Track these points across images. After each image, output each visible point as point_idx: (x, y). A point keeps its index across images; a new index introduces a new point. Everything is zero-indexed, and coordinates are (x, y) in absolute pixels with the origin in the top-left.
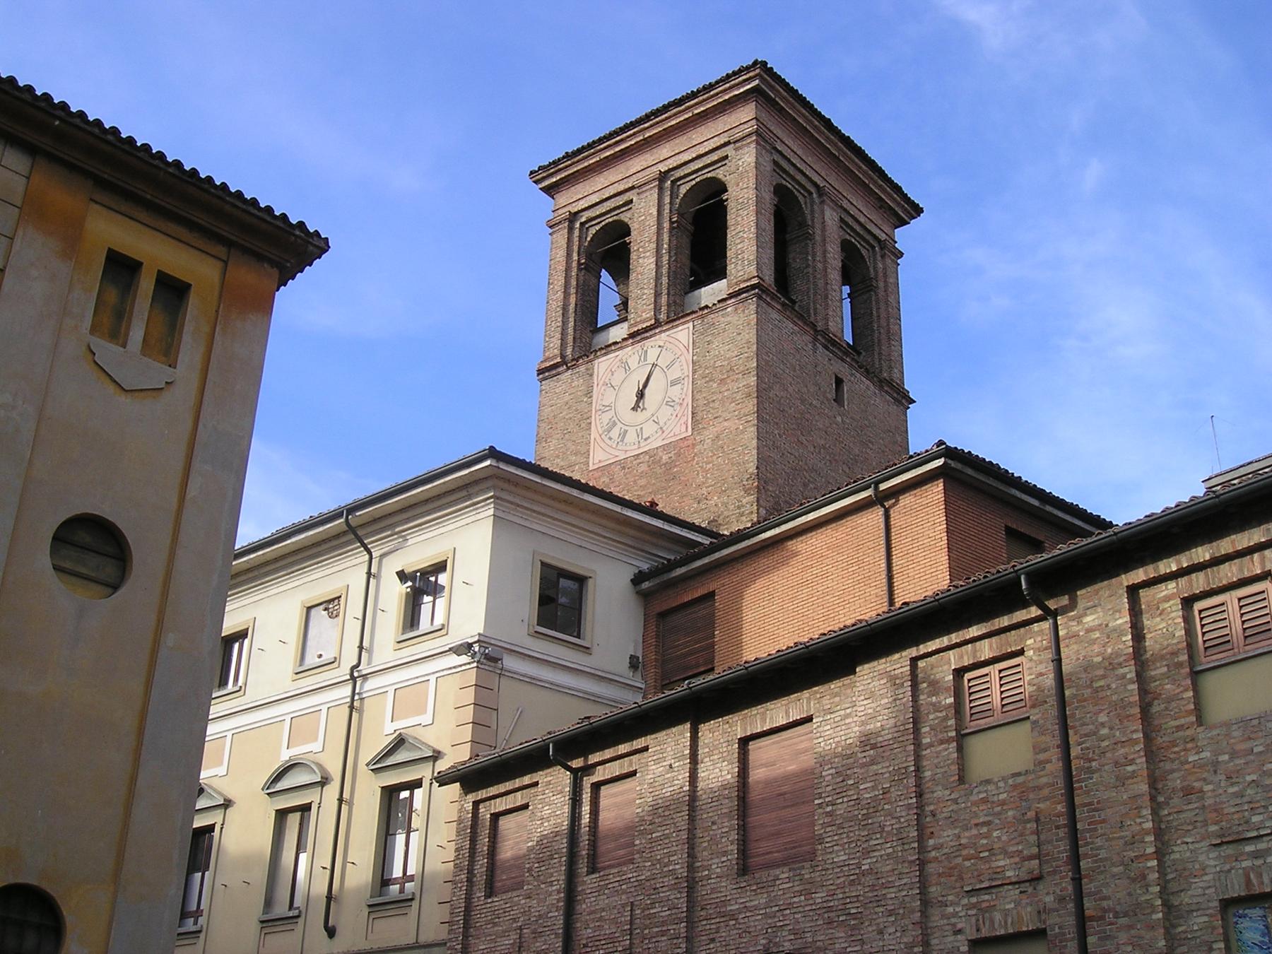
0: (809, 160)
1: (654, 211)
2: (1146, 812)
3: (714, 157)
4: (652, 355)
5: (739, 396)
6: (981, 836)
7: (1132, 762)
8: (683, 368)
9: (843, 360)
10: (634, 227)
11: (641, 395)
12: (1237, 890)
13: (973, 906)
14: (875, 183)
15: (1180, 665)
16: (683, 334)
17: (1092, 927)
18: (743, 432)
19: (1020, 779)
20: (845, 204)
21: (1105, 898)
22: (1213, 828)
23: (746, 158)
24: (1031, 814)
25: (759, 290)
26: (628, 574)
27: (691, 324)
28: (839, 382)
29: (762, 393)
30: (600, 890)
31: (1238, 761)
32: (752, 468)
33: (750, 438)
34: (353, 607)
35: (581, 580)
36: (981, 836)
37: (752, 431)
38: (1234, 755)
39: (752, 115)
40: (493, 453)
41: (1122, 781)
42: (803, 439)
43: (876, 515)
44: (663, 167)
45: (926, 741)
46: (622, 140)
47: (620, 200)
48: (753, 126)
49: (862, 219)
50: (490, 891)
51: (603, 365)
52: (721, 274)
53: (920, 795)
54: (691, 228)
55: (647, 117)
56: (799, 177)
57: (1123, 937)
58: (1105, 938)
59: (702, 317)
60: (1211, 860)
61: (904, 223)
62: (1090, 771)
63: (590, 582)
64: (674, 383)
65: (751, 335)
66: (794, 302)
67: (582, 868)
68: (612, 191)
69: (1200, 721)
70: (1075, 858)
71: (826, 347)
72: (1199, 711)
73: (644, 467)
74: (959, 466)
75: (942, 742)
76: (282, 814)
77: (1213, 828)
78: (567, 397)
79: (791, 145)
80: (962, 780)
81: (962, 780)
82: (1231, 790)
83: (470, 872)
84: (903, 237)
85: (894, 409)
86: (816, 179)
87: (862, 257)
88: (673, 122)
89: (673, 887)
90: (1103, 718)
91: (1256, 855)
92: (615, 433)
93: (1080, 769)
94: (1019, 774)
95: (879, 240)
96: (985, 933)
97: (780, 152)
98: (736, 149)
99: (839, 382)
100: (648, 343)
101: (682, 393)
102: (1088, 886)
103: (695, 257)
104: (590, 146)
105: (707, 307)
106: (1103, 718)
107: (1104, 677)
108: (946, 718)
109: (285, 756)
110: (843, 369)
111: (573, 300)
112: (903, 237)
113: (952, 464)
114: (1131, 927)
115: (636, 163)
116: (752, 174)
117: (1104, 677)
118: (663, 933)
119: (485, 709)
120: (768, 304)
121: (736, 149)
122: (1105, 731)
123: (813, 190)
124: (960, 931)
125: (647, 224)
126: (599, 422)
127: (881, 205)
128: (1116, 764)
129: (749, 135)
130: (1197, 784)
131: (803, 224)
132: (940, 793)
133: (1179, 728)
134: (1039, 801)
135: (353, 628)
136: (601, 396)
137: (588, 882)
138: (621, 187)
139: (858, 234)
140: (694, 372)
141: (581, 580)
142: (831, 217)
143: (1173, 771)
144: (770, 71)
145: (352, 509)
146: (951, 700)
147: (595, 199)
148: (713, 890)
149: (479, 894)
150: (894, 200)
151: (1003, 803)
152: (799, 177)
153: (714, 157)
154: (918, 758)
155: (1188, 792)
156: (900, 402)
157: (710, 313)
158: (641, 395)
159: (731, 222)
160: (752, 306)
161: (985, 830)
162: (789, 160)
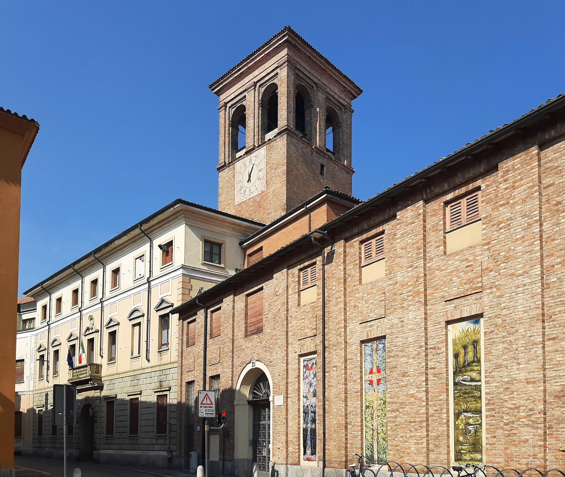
0: (312, 72)
1: (253, 100)
2: (343, 314)
3: (273, 74)
4: (254, 159)
5: (280, 174)
6: (302, 323)
7: (340, 297)
8: (263, 166)
9: (324, 157)
10: (247, 107)
11: (250, 176)
12: (365, 338)
13: (300, 344)
14: (342, 80)
15: (356, 265)
16: (263, 151)
17: (327, 349)
18: (282, 188)
19: (313, 304)
20: (328, 90)
21: (331, 341)
22: (360, 318)
23: (283, 73)
24: (315, 316)
25: (287, 131)
26: (237, 244)
27: (265, 147)
28: (322, 166)
29: (289, 172)
30: (213, 344)
31: (369, 296)
32: (285, 201)
33: (284, 190)
34: (147, 258)
35: (220, 245)
36: (302, 323)
37: (285, 188)
38: (368, 294)
39: (286, 53)
40: (179, 201)
41: (337, 304)
42: (306, 189)
43: (307, 217)
44: (255, 80)
45: (290, 293)
46: (331, 70)
47: (242, 96)
48: (285, 58)
49: (336, 97)
50: (188, 346)
51: (238, 165)
52: (276, 126)
53: (287, 311)
54: (268, 106)
55: (248, 58)
56: (308, 80)
57: (334, 352)
58: (330, 353)
59: (269, 144)
60: (359, 328)
61: (355, 97)
62: (330, 301)
63: (223, 246)
64: (260, 171)
65: (284, 150)
66: (306, 135)
67: (208, 337)
68: (238, 92)
69: (360, 283)
70: (324, 328)
71: (317, 153)
72: (360, 280)
73: (252, 203)
74: (332, 196)
75: (294, 293)
76: (134, 325)
77: (360, 318)
78: (227, 178)
79: (304, 66)
80: (299, 305)
81: (299, 305)
82: (366, 306)
83: (182, 340)
84: (354, 104)
85: (346, 175)
86: (315, 80)
87: (337, 113)
88: (258, 59)
89: (229, 342)
90: (334, 283)
91: (371, 326)
92: (242, 191)
93: (327, 300)
94: (313, 303)
95: (344, 106)
96: (302, 353)
97: (299, 70)
98: (280, 69)
99: (322, 166)
100: (252, 155)
101: (262, 174)
102: (326, 337)
103: (269, 119)
104: (229, 72)
105: (270, 139)
106: (334, 283)
107: (335, 270)
108: (296, 285)
109: (133, 307)
110: (324, 161)
111: (227, 140)
112: (354, 104)
113: (329, 196)
114: (336, 350)
115: (246, 80)
116: (286, 81)
117: (335, 270)
118: (226, 356)
119: (186, 288)
120: (292, 137)
121: (280, 69)
122: (334, 288)
123: (314, 85)
124: (295, 352)
125: (252, 104)
126: (237, 187)
127: (345, 90)
128: (337, 298)
129: (284, 63)
130: (357, 304)
131: (310, 101)
132: (294, 310)
133: (355, 286)
134: (318, 311)
135: (148, 264)
136: (238, 177)
137: (209, 341)
138: (241, 90)
139: (335, 104)
140: (267, 166)
141: (220, 245)
142: (320, 97)
143: (351, 300)
144: (294, 33)
145: (141, 223)
146: (297, 279)
147: (233, 96)
148: (239, 342)
149: (185, 346)
150: (350, 87)
151: (308, 312)
152: (308, 80)
153: (273, 74)
154: (287, 299)
155: (355, 306)
156: (349, 172)
157: (272, 142)
158: (250, 176)
159: (279, 103)
160: (285, 136)
161: (303, 321)
162: (303, 73)
